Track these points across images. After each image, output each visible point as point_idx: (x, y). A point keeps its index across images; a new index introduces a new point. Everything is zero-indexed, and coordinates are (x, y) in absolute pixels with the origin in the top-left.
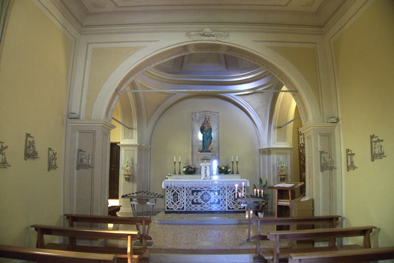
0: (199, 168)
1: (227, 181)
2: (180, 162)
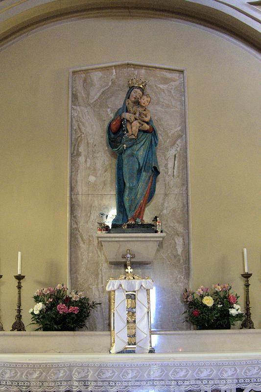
0: (104, 299)
1: (234, 364)
2: (19, 278)
